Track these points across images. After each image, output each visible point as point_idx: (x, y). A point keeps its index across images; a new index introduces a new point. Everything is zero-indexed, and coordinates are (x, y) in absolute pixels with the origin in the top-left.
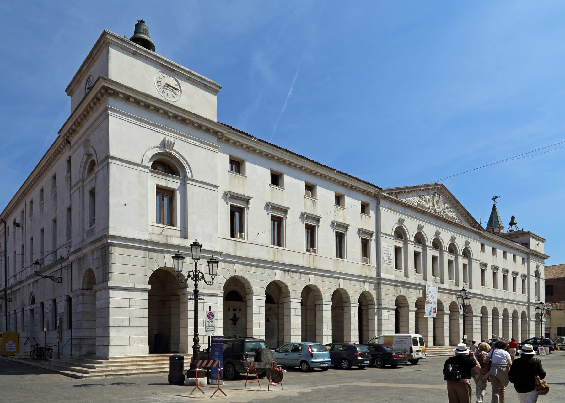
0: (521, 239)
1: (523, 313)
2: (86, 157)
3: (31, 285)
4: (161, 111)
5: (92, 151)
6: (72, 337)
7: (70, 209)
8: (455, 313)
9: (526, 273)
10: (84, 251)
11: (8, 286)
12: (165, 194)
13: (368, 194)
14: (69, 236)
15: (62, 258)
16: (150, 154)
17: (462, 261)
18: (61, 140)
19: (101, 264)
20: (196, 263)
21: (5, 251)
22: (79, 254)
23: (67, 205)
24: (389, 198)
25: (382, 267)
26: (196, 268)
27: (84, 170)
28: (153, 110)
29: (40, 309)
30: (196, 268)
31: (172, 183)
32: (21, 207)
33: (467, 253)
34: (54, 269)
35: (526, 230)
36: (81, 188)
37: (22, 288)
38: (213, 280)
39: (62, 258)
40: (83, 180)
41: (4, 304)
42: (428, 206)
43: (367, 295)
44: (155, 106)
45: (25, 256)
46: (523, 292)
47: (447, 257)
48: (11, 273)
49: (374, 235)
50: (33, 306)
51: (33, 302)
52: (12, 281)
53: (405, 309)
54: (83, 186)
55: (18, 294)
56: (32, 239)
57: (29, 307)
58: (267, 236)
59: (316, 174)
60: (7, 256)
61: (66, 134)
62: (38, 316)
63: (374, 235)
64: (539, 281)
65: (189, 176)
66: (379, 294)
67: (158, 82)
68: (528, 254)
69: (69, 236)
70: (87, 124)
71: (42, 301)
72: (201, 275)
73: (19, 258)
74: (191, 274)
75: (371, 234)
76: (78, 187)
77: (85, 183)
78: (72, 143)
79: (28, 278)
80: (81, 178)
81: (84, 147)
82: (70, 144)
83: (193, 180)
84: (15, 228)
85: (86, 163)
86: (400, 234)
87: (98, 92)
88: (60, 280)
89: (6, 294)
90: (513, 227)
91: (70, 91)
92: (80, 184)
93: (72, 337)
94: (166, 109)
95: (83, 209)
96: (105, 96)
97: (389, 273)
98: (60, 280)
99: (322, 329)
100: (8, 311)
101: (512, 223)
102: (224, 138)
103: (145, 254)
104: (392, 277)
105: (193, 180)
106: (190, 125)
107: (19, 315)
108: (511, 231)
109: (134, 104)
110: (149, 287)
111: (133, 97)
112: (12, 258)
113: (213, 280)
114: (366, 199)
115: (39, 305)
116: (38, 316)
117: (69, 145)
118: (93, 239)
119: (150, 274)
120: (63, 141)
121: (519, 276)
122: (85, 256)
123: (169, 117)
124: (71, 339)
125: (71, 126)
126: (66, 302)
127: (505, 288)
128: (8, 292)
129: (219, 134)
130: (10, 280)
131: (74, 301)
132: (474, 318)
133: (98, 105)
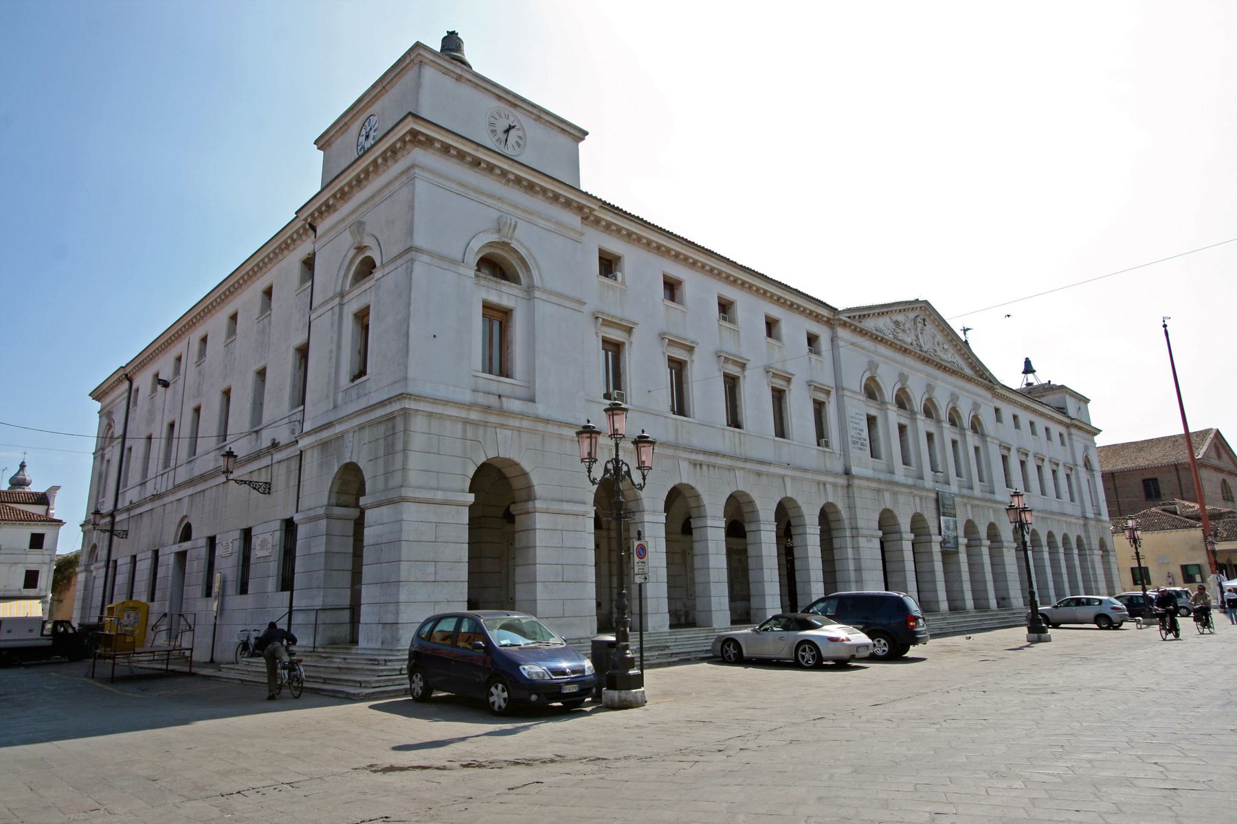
0: (1049, 398)
1: (1079, 539)
2: (353, 252)
3: (186, 500)
4: (498, 171)
5: (368, 241)
6: (291, 606)
7: (303, 352)
8: (923, 538)
9: (1070, 461)
10: (338, 429)
11: (119, 506)
12: (497, 317)
13: (817, 318)
14: (300, 398)
15: (275, 445)
16: (476, 245)
17: (972, 440)
18: (299, 224)
19: (381, 452)
20: (617, 445)
21: (124, 436)
22: (325, 434)
23: (299, 339)
24: (851, 325)
25: (852, 455)
26: (617, 455)
27: (346, 276)
28: (484, 169)
29: (204, 552)
30: (617, 455)
31: (504, 294)
32: (178, 348)
33: (976, 426)
34: (255, 466)
35: (1057, 382)
36: (337, 309)
37: (160, 510)
38: (644, 479)
39: (275, 445)
40: (342, 295)
41: (106, 543)
42: (909, 340)
43: (787, 506)
44: (488, 163)
45: (175, 441)
46: (1072, 500)
47: (949, 433)
48: (134, 476)
49: (833, 392)
50: (186, 545)
51: (186, 534)
52: (131, 495)
53: (897, 536)
54: (341, 305)
55: (146, 520)
56: (197, 410)
57: (176, 548)
58: (663, 398)
59: (735, 281)
60: (127, 445)
61: (312, 215)
62: (196, 566)
63: (833, 392)
64: (1093, 476)
65: (537, 282)
66: (851, 508)
67: (492, 124)
68: (1068, 426)
69: (300, 398)
70: (359, 197)
71: (211, 534)
72: (625, 468)
73: (158, 446)
74: (610, 466)
75: (828, 393)
76: (329, 306)
77: (346, 299)
78: (319, 231)
79: (177, 487)
80: (338, 289)
81: (352, 234)
82: (315, 231)
83: (545, 291)
84: (154, 390)
85: (352, 262)
86: (872, 391)
87: (399, 140)
88: (267, 488)
89: (113, 523)
90: (1031, 378)
91: (323, 142)
92: (337, 300)
93: (291, 606)
94: (505, 166)
95: (339, 348)
96: (409, 146)
97: (862, 465)
98: (267, 488)
99: (762, 582)
100: (113, 558)
101: (1028, 369)
102: (592, 218)
103: (465, 431)
104: (869, 473)
105: (545, 291)
106: (540, 196)
107: (144, 566)
108: (1029, 384)
109: (455, 160)
110: (471, 498)
111: (455, 148)
112: (138, 447)
113: (644, 479)
114: (816, 328)
115: (202, 542)
116: (196, 566)
117: (311, 232)
118: (363, 403)
119: (471, 472)
120: (303, 227)
121: (1046, 463)
122: (340, 437)
123: (509, 180)
124: (290, 613)
125: (327, 200)
126: (278, 534)
127: (1043, 493)
128: (117, 519)
129: (586, 210)
130: (128, 494)
131: (302, 531)
132: (1005, 550)
133: (390, 162)
